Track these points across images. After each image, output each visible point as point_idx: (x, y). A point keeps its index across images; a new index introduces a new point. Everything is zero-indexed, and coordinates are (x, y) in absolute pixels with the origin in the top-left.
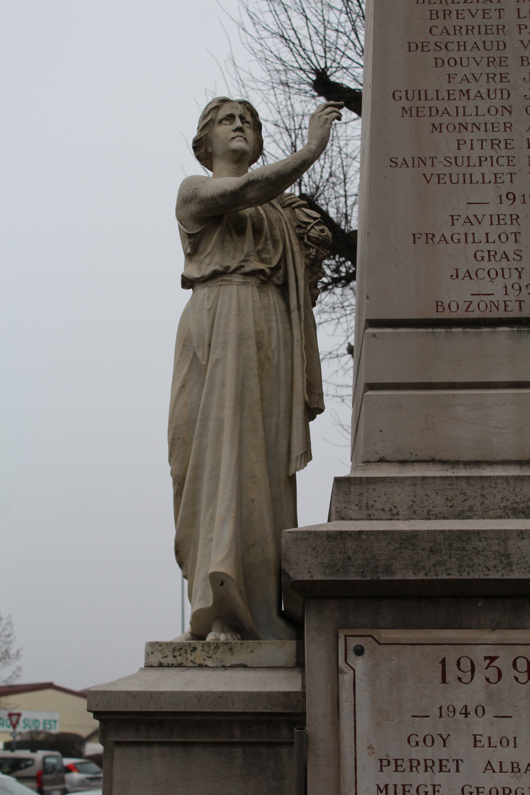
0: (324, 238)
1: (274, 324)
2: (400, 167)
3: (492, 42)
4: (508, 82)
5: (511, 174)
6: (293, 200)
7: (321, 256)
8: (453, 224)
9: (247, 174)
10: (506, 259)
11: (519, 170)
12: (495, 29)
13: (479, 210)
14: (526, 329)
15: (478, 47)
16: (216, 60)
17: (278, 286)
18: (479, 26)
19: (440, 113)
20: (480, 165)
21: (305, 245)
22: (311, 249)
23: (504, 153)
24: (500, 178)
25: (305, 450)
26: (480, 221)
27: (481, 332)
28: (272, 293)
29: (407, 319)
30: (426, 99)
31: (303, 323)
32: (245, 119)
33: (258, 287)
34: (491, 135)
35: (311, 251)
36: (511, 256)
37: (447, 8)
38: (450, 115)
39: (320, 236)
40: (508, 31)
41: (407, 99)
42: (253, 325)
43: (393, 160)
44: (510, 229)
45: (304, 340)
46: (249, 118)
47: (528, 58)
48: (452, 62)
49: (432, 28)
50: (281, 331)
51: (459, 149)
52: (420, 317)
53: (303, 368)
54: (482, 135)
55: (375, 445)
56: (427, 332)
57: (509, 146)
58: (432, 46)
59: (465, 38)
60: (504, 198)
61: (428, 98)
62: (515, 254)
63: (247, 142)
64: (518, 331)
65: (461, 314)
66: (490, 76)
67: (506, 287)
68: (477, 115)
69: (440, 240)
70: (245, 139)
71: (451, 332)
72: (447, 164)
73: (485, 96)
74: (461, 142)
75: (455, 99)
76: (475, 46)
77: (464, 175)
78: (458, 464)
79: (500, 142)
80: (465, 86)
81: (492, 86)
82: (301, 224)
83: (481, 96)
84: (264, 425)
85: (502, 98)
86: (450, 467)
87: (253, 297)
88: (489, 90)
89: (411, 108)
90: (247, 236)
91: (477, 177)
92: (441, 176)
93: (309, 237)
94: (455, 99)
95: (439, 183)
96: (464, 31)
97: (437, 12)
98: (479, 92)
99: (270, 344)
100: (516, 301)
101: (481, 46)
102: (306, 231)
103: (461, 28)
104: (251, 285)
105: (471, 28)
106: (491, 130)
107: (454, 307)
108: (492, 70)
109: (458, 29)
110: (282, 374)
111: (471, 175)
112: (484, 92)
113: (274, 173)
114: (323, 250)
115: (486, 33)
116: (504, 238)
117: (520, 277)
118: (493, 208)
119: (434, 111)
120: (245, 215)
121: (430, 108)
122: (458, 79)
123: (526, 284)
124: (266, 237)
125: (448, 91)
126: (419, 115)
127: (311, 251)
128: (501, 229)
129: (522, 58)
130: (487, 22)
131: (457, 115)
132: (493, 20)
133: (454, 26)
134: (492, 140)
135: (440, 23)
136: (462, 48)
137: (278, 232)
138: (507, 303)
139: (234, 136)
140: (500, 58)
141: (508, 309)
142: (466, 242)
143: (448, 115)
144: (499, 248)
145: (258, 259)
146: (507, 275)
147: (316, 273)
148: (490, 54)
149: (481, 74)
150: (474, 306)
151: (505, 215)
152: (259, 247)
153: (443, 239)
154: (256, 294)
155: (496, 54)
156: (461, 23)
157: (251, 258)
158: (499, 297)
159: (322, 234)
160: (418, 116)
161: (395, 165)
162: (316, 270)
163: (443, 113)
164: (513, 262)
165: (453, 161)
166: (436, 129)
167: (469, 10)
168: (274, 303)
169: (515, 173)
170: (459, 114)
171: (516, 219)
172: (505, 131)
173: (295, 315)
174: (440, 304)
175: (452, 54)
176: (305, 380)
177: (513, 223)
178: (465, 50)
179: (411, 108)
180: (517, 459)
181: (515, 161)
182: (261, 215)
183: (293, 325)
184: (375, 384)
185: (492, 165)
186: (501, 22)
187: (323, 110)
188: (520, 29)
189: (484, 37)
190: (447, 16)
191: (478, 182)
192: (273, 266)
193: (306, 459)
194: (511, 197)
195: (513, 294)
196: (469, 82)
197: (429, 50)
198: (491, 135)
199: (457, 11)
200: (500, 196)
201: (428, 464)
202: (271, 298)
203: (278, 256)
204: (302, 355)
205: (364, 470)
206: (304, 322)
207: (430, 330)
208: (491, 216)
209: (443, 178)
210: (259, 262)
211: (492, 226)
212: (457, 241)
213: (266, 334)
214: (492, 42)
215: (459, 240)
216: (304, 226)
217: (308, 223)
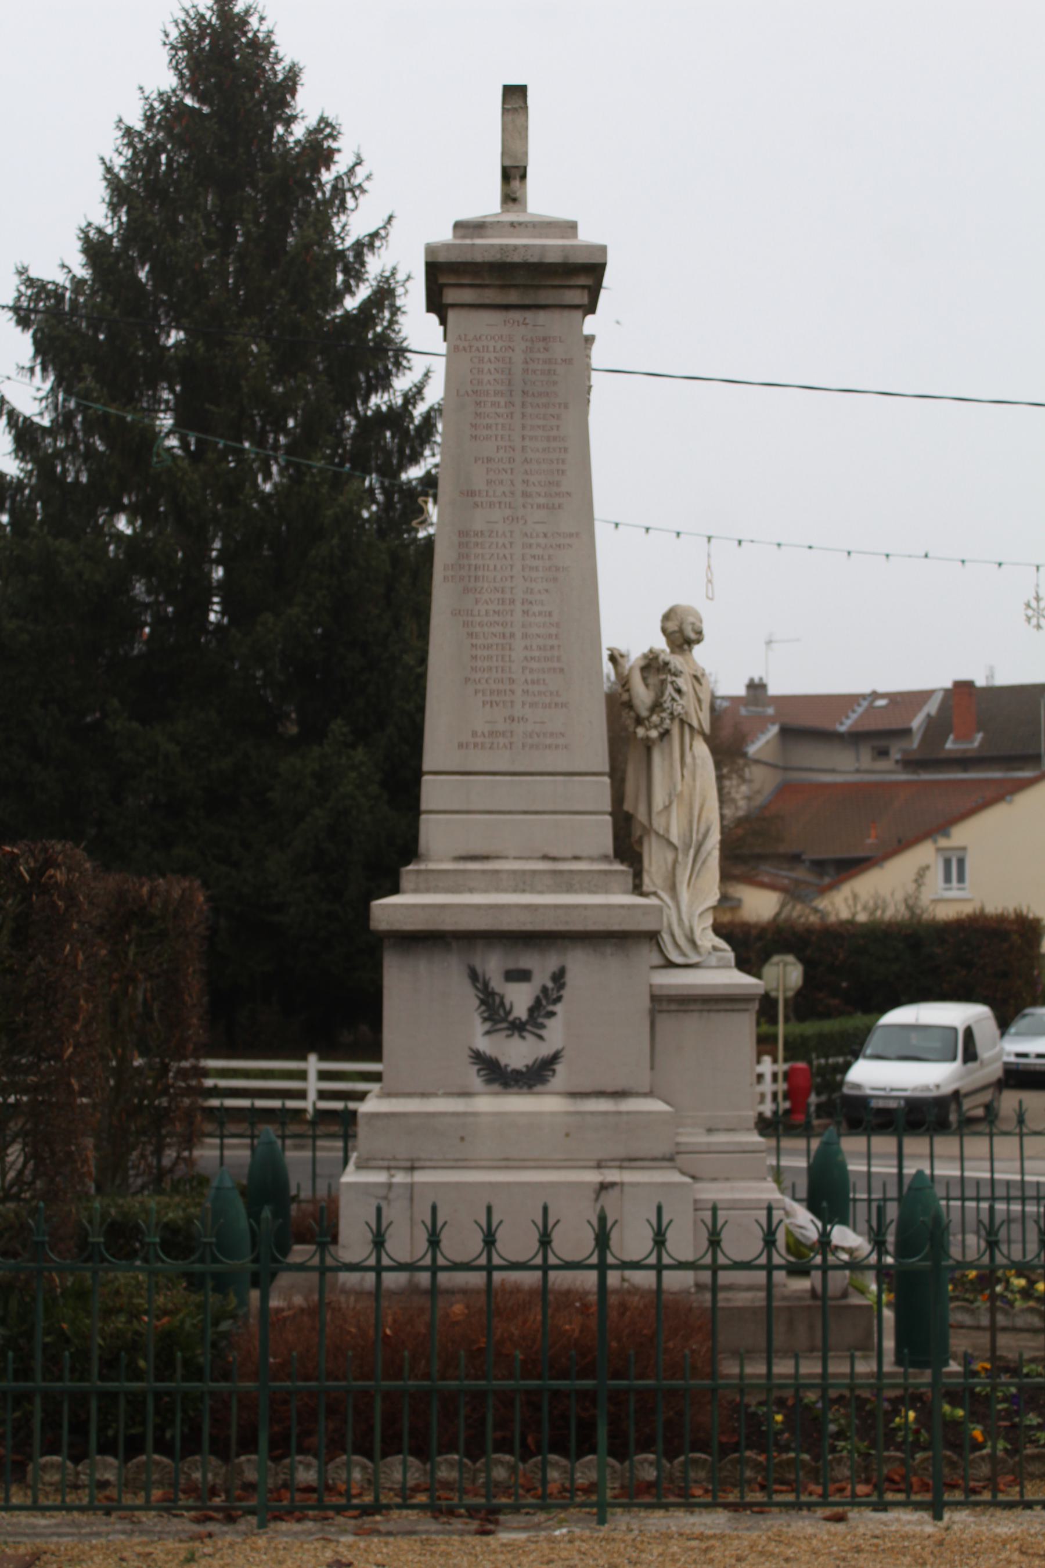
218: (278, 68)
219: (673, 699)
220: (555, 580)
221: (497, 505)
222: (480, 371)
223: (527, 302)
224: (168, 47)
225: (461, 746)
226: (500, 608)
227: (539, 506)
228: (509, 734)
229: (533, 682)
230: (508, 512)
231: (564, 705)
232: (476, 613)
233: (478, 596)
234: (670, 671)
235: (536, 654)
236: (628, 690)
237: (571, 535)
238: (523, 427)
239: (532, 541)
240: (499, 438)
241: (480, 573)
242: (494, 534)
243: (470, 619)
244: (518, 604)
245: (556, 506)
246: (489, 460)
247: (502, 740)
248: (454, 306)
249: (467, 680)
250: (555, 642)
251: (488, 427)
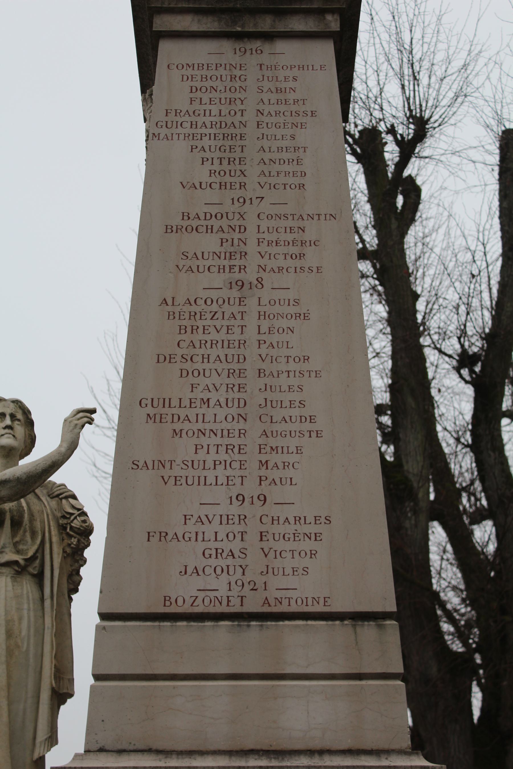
0: (85, 528)
1: (25, 612)
2: (141, 469)
3: (233, 355)
4: (246, 392)
5: (242, 477)
6: (61, 491)
7: (83, 545)
8: (185, 524)
9: (17, 467)
10: (232, 557)
11: (249, 473)
12: (236, 344)
13: (210, 511)
14: (246, 624)
15: (220, 360)
16: (117, 302)
17: (33, 575)
18: (223, 341)
19: (181, 420)
20: (215, 468)
21: (68, 534)
22: (73, 538)
23: (237, 457)
24: (232, 480)
25: (50, 734)
26: (211, 520)
27: (204, 626)
28: (26, 583)
29: (136, 613)
30: (170, 407)
31: (55, 611)
32: (16, 417)
33: (12, 577)
34: (227, 441)
35: (72, 541)
36: (237, 553)
37: (195, 323)
38: (190, 422)
39: (81, 526)
40: (248, 346)
41: (152, 406)
42: (3, 614)
43: (135, 462)
44: (237, 528)
45: (54, 627)
46: (20, 416)
47: (265, 371)
48: (196, 373)
49: (180, 342)
50: (32, 619)
51: (196, 453)
52: (149, 611)
53: (52, 655)
54: (218, 440)
55: (96, 734)
56: (153, 626)
57: (242, 451)
58: (178, 358)
59: (209, 351)
60: (234, 499)
61: (172, 406)
62: (240, 552)
63: (16, 438)
64: (238, 625)
65: (187, 609)
66: (229, 386)
67: (230, 583)
68: (215, 422)
69: (172, 538)
70: (14, 436)
71: (176, 626)
72: (185, 467)
73: (223, 404)
74: (198, 447)
75: (196, 407)
76: (218, 359)
77: (199, 477)
78: (171, 754)
79: (234, 447)
80: (206, 395)
81: (231, 395)
82: (66, 515)
83: (220, 405)
84: (10, 711)
85: (239, 407)
86: (164, 757)
87: (6, 586)
88: (227, 399)
89: (155, 414)
90: (5, 529)
91: (211, 480)
92: (178, 478)
93: (72, 528)
94: (196, 407)
95: (176, 484)
96: (208, 345)
97: (186, 327)
98: (218, 400)
99: (20, 632)
100: (238, 596)
101: (223, 358)
102: (69, 522)
103: (206, 342)
104: (5, 575)
105: (216, 342)
106: (227, 436)
107: (180, 602)
108: (231, 380)
109: (203, 343)
110: (31, 660)
111: (205, 477)
112: (223, 401)
113: (25, 473)
114: (84, 539)
115: (229, 347)
116: (231, 536)
117: (244, 574)
118: (223, 509)
119: (176, 418)
120: (4, 509)
121: (173, 415)
122: (201, 388)
123: (248, 581)
124: (25, 529)
125: (190, 399)
126: (162, 421)
127: (72, 541)
128: (229, 528)
129: (259, 370)
130: (230, 337)
131: (197, 422)
132: (236, 336)
133: (200, 341)
134: (227, 445)
135: (187, 337)
136: (206, 360)
137: (39, 523)
138: (230, 598)
139: (3, 433)
140: (240, 370)
141: (230, 604)
142: (196, 540)
143: (188, 421)
144: (227, 546)
145: (14, 550)
146: (231, 573)
147: (77, 561)
148: (230, 366)
149: (222, 384)
150: (199, 601)
151: (234, 515)
152: (17, 539)
153: (175, 537)
154: (10, 584)
155: (235, 366)
156: (208, 338)
157: (7, 550)
158: (223, 592)
159: (84, 525)
160: (161, 422)
161: (136, 467)
162: (78, 558)
163: (184, 420)
164: (238, 559)
165: (190, 464)
166: (176, 435)
167: (215, 326)
168: (28, 593)
169: (246, 477)
170: (198, 421)
171: (244, 520)
172: (240, 437)
173: (47, 603)
174: (167, 598)
175: (196, 366)
176: (53, 666)
177: (241, 523)
178: (208, 362)
179: (155, 414)
180: (229, 749)
181: (246, 465)
182: (23, 507)
183: (46, 613)
184: (101, 675)
185: (225, 469)
186: (242, 337)
187: (75, 415)
188: (259, 344)
189: (227, 351)
190: (194, 331)
191: (211, 485)
192: (28, 557)
193: (50, 744)
194: (241, 498)
195: (236, 590)
196: (210, 391)
197: (176, 362)
198: (227, 441)
199: (204, 326)
200: (231, 497)
201: (143, 754)
202: (25, 587)
203: (35, 547)
204: (52, 641)
205: (82, 759)
206: (56, 610)
207: (157, 624)
208: (221, 516)
209: (180, 480)
210: (14, 553)
212: (188, 539)
213: (16, 623)
214: (233, 355)
215: (190, 538)
216: (68, 516)
217: (72, 514)
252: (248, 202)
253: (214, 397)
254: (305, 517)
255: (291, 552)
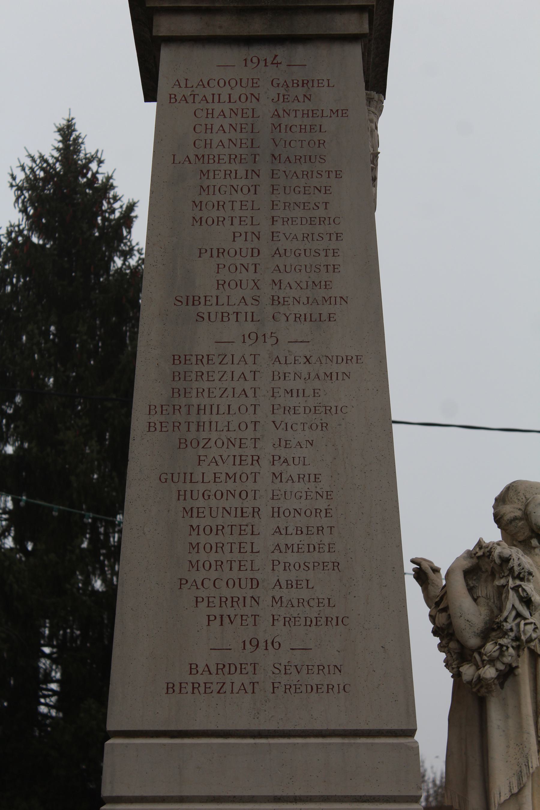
211: (256, 274)
215: (300, 270)
218: (117, 205)
219: (519, 615)
220: (324, 426)
221: (233, 317)
222: (208, 128)
223: (279, 32)
224: (14, 188)
225: (170, 688)
226: (238, 469)
227: (297, 318)
228: (250, 669)
229: (289, 585)
230: (250, 327)
231: (340, 621)
232: (198, 477)
233: (201, 452)
234: (512, 570)
235: (294, 540)
236: (446, 609)
237: (348, 359)
238: (273, 205)
239: (290, 369)
240: (236, 221)
241: (205, 418)
242: (228, 359)
243: (188, 486)
244: (265, 463)
245: (325, 317)
246: (221, 252)
247: (238, 679)
248: (170, 40)
249: (182, 582)
250: (325, 522)
251: (220, 205)
252: (261, 339)
253: (218, 108)
254: (236, 171)
255: (253, 616)
